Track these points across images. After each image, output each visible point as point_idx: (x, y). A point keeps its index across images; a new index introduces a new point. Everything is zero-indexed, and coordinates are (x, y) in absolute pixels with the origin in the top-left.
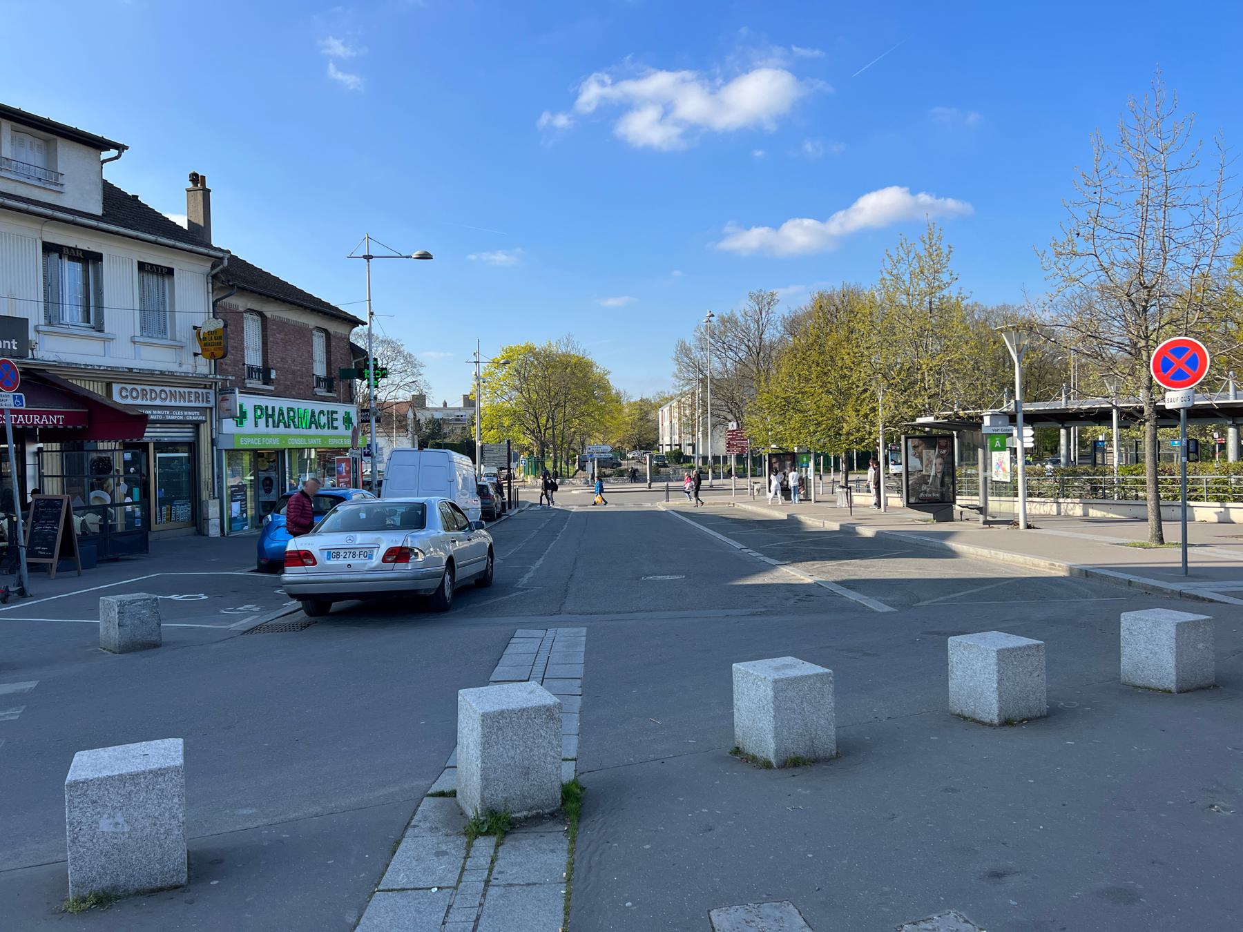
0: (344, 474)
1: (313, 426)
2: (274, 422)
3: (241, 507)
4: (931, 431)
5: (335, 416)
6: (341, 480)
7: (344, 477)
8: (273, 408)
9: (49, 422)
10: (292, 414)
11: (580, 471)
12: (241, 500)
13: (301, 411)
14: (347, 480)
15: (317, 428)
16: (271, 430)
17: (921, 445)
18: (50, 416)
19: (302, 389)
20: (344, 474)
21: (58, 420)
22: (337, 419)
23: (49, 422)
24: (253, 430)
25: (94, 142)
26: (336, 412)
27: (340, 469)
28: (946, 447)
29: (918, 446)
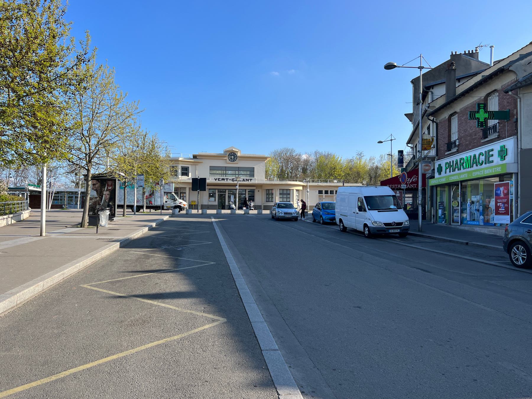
0: (502, 195)
1: (475, 165)
2: (453, 169)
3: (442, 212)
4: (260, 214)
5: (491, 153)
6: (499, 201)
7: (502, 198)
8: (453, 161)
9: (410, 187)
10: (462, 161)
11: (279, 396)
12: (442, 209)
13: (466, 158)
14: (505, 200)
15: (477, 165)
16: (452, 173)
17: (97, 184)
18: (411, 185)
19: (475, 143)
20: (502, 195)
21: (414, 186)
22: (492, 155)
23: (410, 187)
24: (445, 175)
25: (512, 85)
26: (492, 150)
27: (498, 192)
28: (111, 185)
29: (96, 184)
